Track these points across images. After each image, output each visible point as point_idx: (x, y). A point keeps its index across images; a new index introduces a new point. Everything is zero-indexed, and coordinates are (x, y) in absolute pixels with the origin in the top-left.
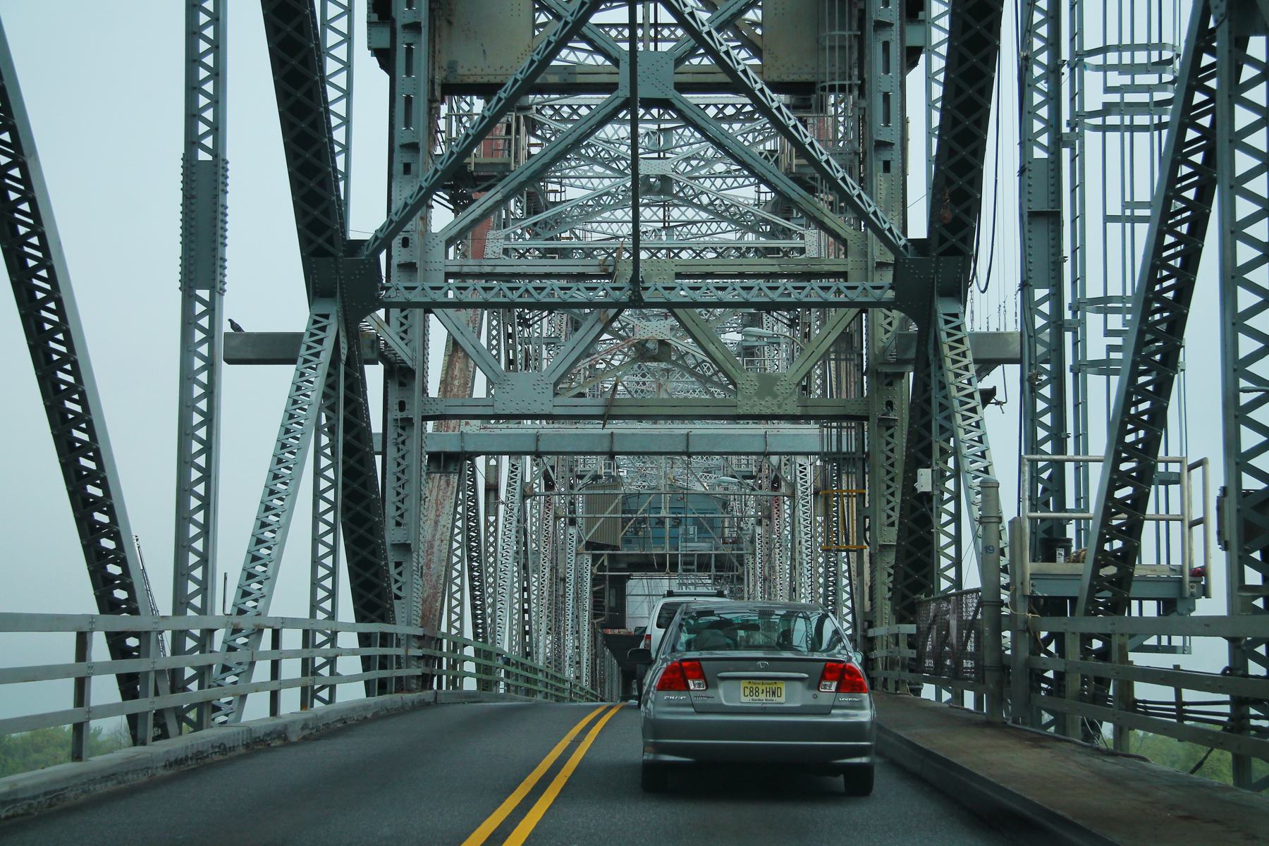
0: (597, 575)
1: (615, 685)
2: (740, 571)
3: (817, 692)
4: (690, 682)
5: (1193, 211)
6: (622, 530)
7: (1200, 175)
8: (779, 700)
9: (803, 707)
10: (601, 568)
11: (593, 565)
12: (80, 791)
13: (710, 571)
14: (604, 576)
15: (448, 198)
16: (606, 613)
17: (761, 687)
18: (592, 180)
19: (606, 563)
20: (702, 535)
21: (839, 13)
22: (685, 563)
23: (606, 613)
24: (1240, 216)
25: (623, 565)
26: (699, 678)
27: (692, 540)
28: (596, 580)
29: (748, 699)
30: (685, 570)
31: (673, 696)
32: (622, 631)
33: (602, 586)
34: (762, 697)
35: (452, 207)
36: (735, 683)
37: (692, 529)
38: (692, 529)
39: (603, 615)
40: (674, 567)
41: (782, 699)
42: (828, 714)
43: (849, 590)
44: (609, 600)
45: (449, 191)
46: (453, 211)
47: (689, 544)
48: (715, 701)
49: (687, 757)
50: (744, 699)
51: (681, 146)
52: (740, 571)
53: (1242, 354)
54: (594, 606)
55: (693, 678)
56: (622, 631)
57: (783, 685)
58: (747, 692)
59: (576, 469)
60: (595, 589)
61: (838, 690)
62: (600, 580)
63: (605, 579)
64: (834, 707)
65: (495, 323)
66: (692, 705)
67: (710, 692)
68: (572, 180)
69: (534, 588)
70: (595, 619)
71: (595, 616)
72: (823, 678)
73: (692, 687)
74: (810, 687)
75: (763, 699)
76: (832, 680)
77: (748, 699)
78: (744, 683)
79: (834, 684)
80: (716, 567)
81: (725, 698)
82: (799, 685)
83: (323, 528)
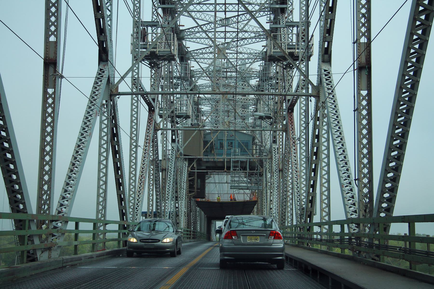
0: (190, 172)
2: (261, 170)
4: (233, 237)
5: (415, 67)
6: (203, 149)
7: (418, 53)
8: (257, 241)
10: (193, 168)
11: (188, 167)
13: (246, 170)
14: (194, 172)
15: (148, 63)
16: (195, 190)
17: (253, 238)
18: (197, 39)
19: (195, 166)
20: (242, 153)
22: (234, 167)
23: (195, 190)
25: (204, 168)
27: (238, 155)
28: (190, 174)
30: (234, 170)
32: (204, 200)
33: (193, 178)
34: (253, 241)
35: (150, 66)
36: (246, 236)
37: (237, 150)
38: (237, 150)
39: (193, 192)
40: (229, 168)
41: (259, 241)
44: (197, 183)
45: (149, 61)
46: (150, 68)
47: (236, 157)
50: (248, 241)
51: (232, 48)
52: (261, 170)
54: (189, 187)
55: (234, 236)
56: (204, 200)
57: (259, 237)
58: (249, 239)
59: (175, 112)
60: (190, 179)
61: (274, 238)
62: (193, 174)
63: (194, 174)
64: (273, 243)
66: (234, 243)
68: (190, 39)
70: (190, 193)
71: (190, 192)
72: (270, 235)
74: (266, 238)
76: (272, 236)
78: (248, 237)
79: (273, 237)
80: (249, 168)
82: (263, 237)
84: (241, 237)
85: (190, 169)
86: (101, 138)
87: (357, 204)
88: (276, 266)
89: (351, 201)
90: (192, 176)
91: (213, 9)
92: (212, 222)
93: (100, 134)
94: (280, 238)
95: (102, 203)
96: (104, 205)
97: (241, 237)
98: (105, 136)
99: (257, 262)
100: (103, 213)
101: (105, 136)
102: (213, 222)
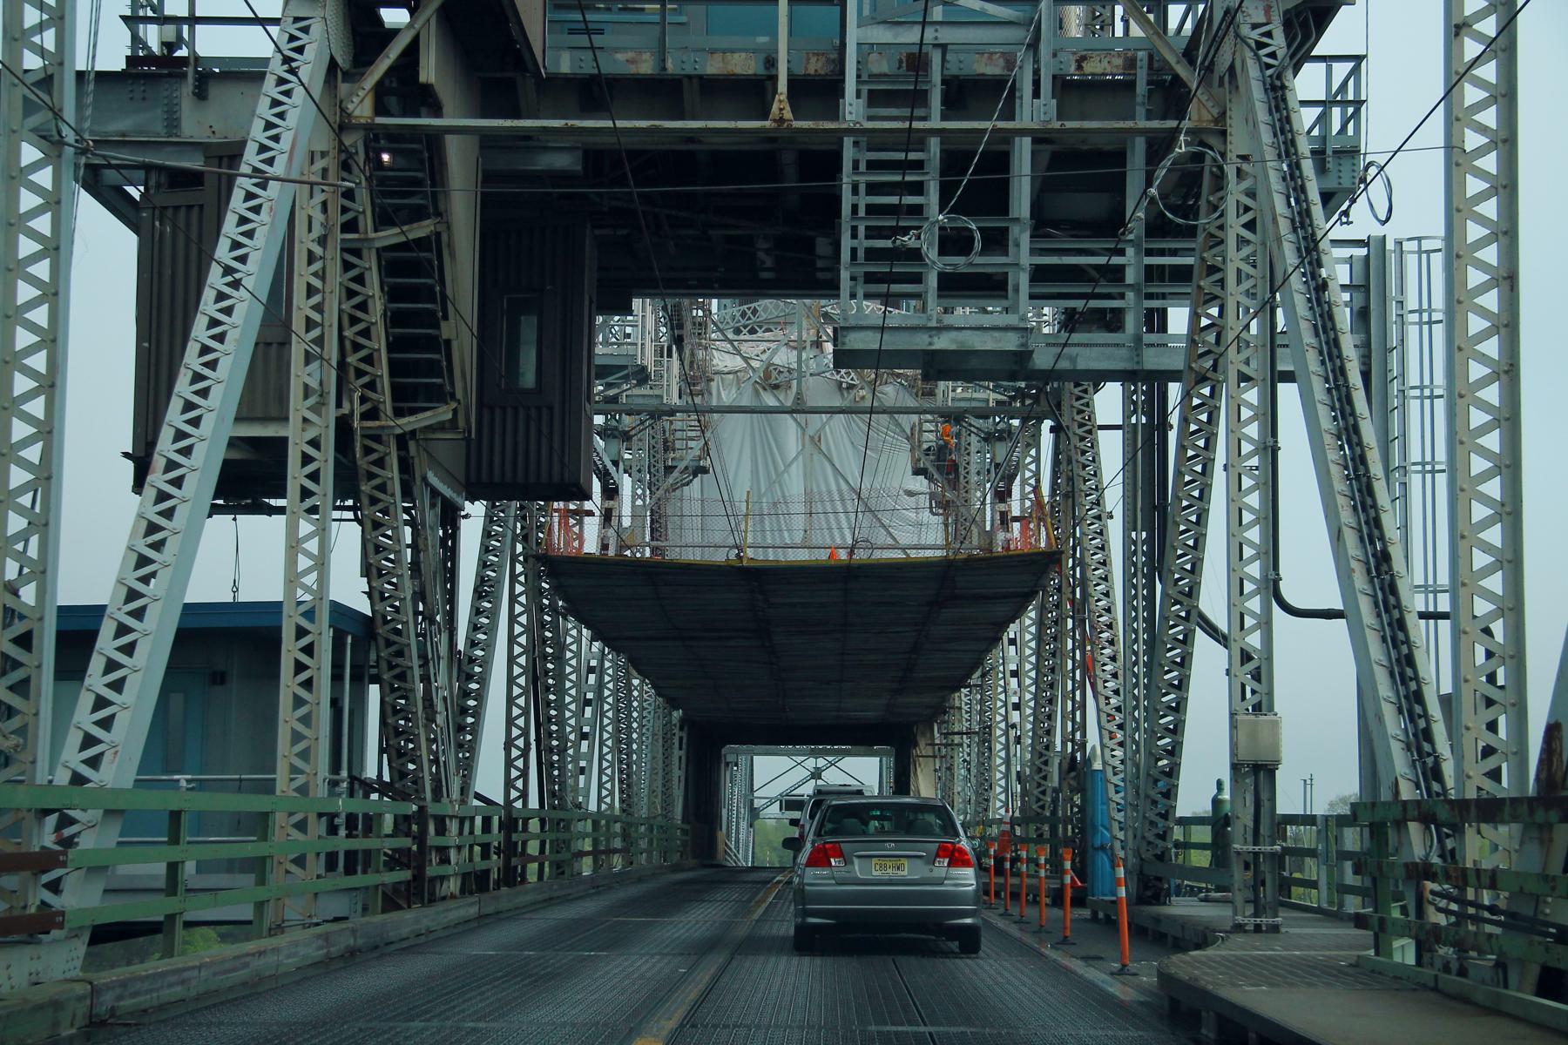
1: (677, 753)
3: (931, 866)
4: (832, 860)
8: (902, 873)
9: (922, 878)
12: (356, 1030)
21: (401, 333)
24: (43, 355)
26: (839, 857)
29: (879, 873)
31: (818, 871)
34: (890, 871)
36: (867, 860)
41: (905, 873)
42: (942, 884)
43: (1003, 799)
48: (852, 875)
49: (823, 918)
50: (874, 873)
53: (45, 308)
55: (834, 857)
57: (905, 862)
58: (878, 867)
61: (949, 865)
64: (946, 879)
65: (639, 492)
66: (834, 878)
67: (849, 867)
69: (610, 672)
72: (938, 855)
73: (833, 864)
74: (927, 863)
75: (891, 873)
76: (944, 857)
77: (879, 873)
78: (874, 861)
79: (947, 860)
81: (860, 870)
82: (918, 862)
83: (516, 712)
84: (856, 861)
85: (361, 107)
86: (511, 680)
87: (1121, 673)
88: (955, 945)
89: (1102, 587)
90: (418, 214)
91: (822, 420)
92: (730, 758)
93: (510, 670)
94: (966, 864)
95: (26, 500)
96: (37, 509)
97: (856, 861)
98: (606, 769)
99: (905, 935)
100: (33, 552)
101: (606, 769)
102: (729, 751)
